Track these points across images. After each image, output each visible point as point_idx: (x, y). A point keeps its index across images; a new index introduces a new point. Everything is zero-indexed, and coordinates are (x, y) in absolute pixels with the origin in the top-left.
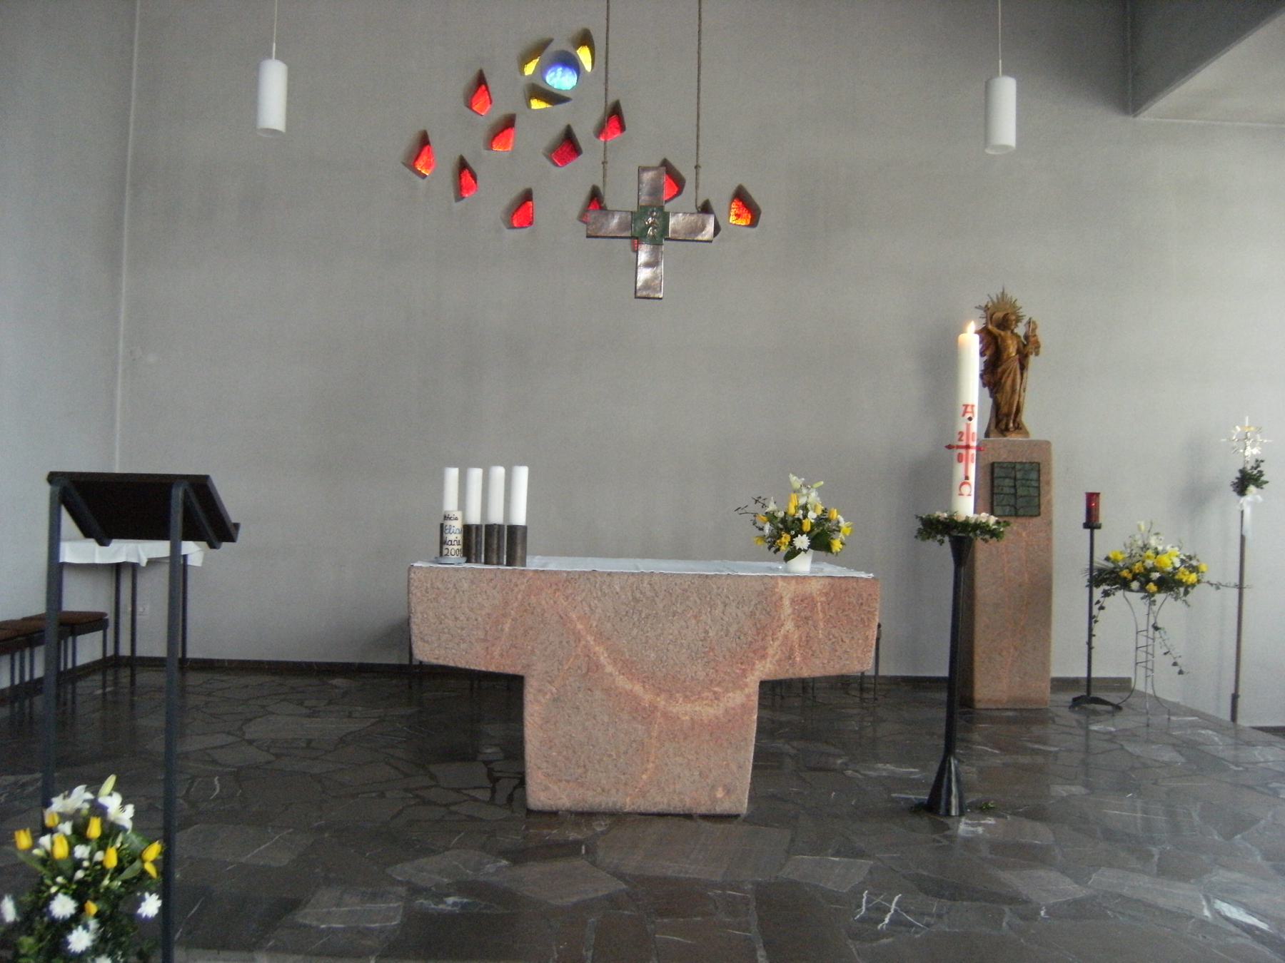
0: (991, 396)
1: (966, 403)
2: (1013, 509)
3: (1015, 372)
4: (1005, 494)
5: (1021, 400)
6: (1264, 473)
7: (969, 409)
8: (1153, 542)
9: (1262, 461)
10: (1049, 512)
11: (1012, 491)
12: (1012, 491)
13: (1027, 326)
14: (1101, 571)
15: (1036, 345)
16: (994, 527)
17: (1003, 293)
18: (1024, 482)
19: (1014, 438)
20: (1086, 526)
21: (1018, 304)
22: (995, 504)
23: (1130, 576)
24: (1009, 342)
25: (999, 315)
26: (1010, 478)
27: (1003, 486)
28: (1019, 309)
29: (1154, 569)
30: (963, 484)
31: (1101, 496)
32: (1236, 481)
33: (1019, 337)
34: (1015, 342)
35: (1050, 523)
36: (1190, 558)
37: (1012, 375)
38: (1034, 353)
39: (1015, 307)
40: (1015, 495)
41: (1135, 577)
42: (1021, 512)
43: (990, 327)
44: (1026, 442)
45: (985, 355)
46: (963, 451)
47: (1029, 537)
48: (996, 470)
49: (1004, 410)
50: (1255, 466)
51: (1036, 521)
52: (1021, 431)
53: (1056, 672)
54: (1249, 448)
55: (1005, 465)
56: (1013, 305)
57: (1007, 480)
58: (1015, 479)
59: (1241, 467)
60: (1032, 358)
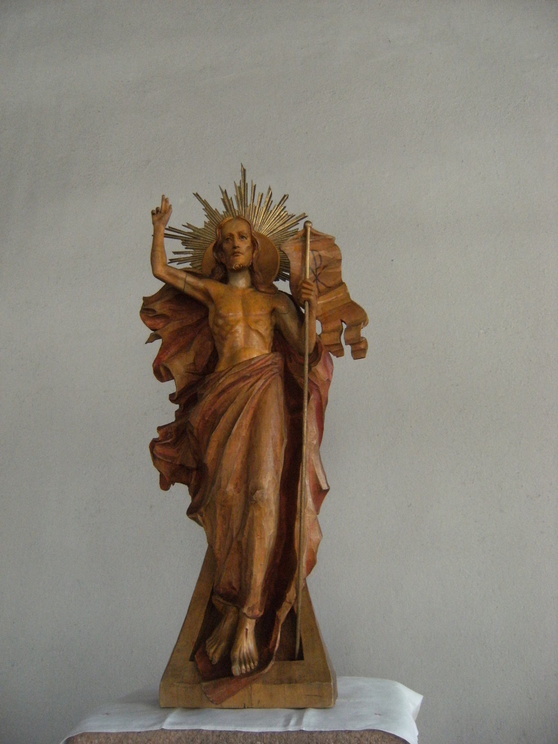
38: (347, 349)
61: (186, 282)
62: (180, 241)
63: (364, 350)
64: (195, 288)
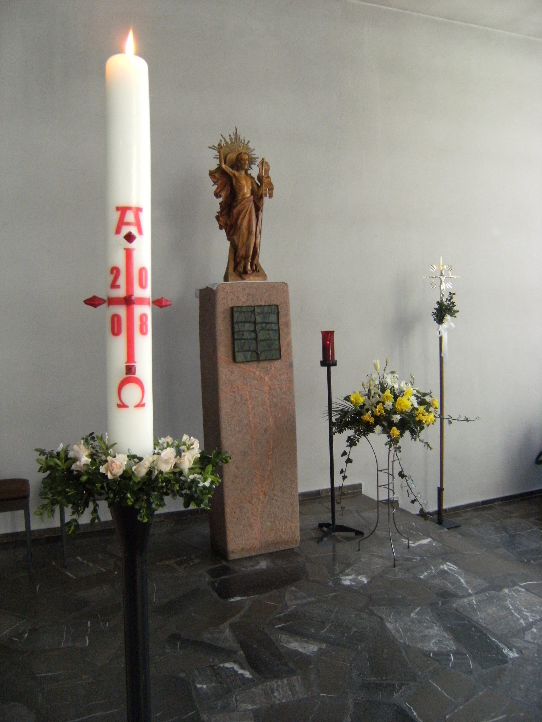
0: (229, 239)
1: (123, 203)
2: (254, 354)
3: (251, 210)
4: (245, 339)
5: (258, 241)
6: (455, 304)
7: (130, 217)
8: (389, 380)
9: (454, 294)
10: (290, 354)
11: (253, 335)
12: (253, 335)
13: (260, 166)
14: (344, 413)
15: (270, 187)
16: (191, 477)
17: (236, 134)
18: (264, 325)
19: (252, 280)
20: (323, 364)
21: (251, 146)
22: (236, 350)
23: (372, 420)
24: (244, 182)
25: (232, 156)
26: (250, 322)
27: (243, 331)
28: (252, 151)
29: (394, 411)
30: (123, 383)
31: (335, 334)
32: (435, 311)
33: (252, 178)
34: (249, 183)
35: (291, 365)
36: (425, 394)
37: (247, 216)
38: (268, 195)
39: (248, 148)
40: (256, 339)
41: (378, 420)
42: (262, 357)
43: (224, 166)
44: (264, 284)
45: (220, 196)
46: (121, 311)
47: (271, 380)
48: (236, 315)
49: (242, 252)
50: (449, 298)
51: (277, 364)
52: (258, 274)
53: (303, 488)
54: (443, 283)
55: (244, 309)
56: (247, 147)
57: (247, 325)
58: (255, 323)
59: (439, 300)
60: (266, 200)
61: (230, 171)
62: (217, 151)
63: (272, 196)
64: (231, 172)
